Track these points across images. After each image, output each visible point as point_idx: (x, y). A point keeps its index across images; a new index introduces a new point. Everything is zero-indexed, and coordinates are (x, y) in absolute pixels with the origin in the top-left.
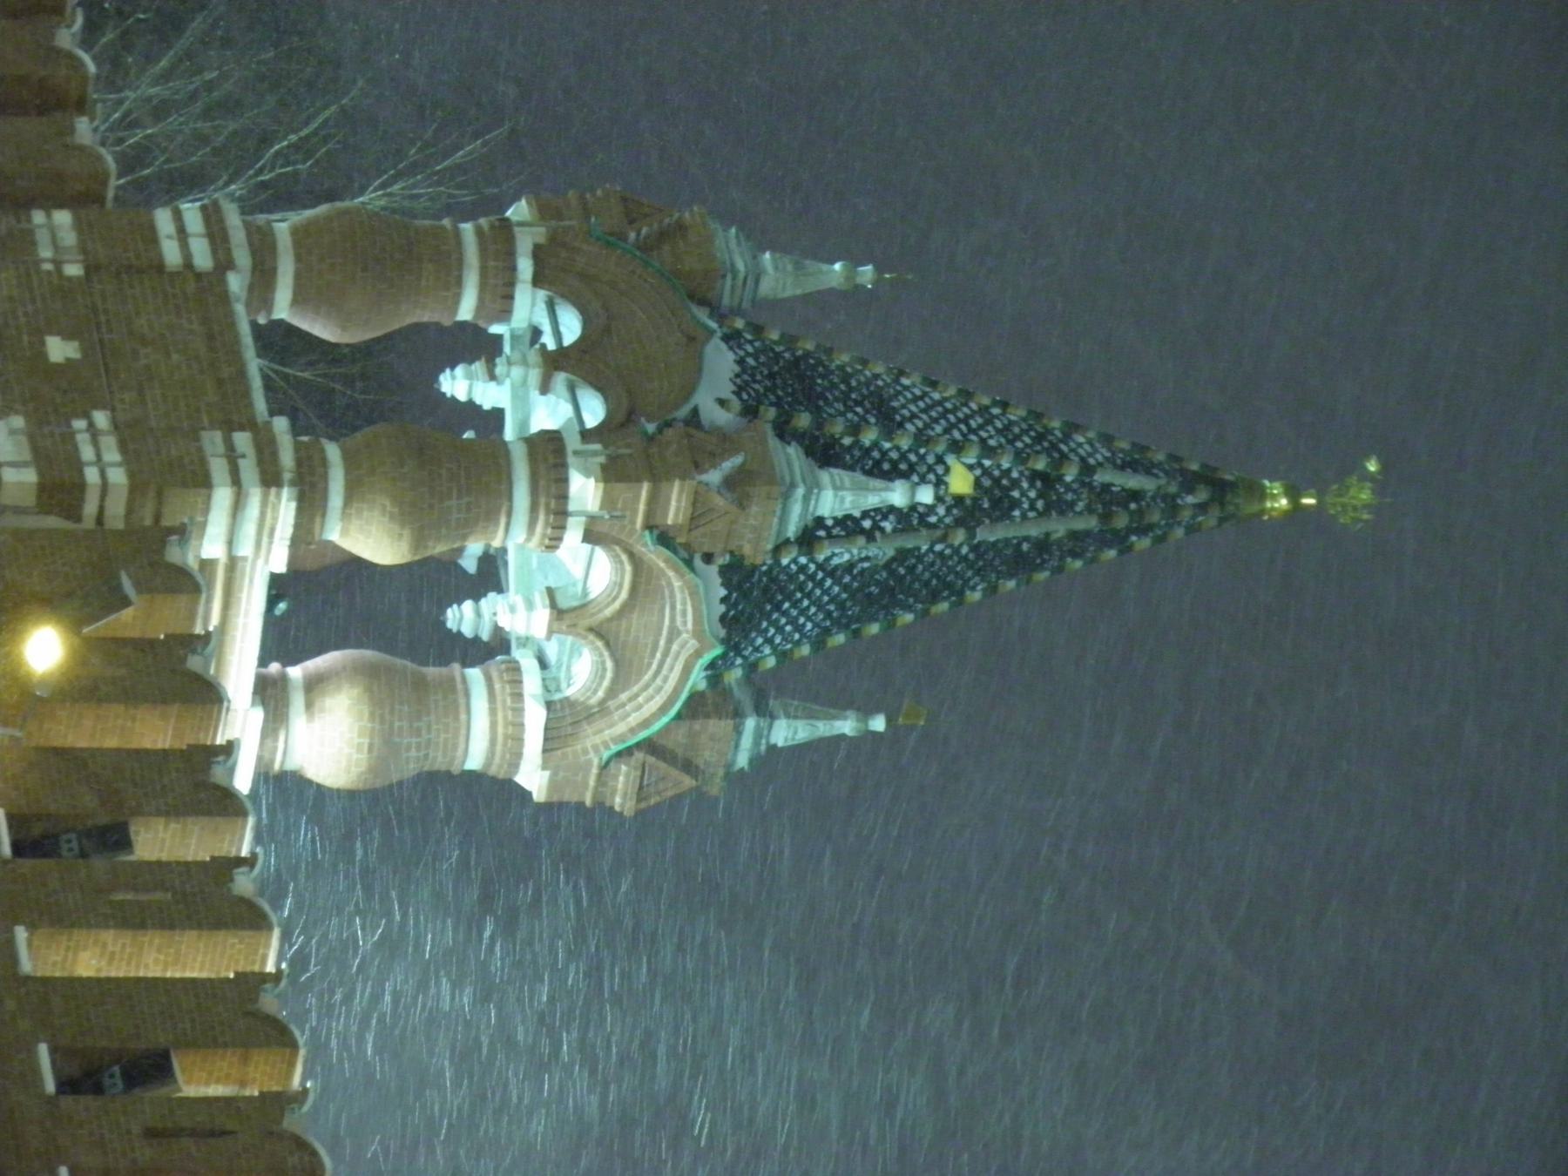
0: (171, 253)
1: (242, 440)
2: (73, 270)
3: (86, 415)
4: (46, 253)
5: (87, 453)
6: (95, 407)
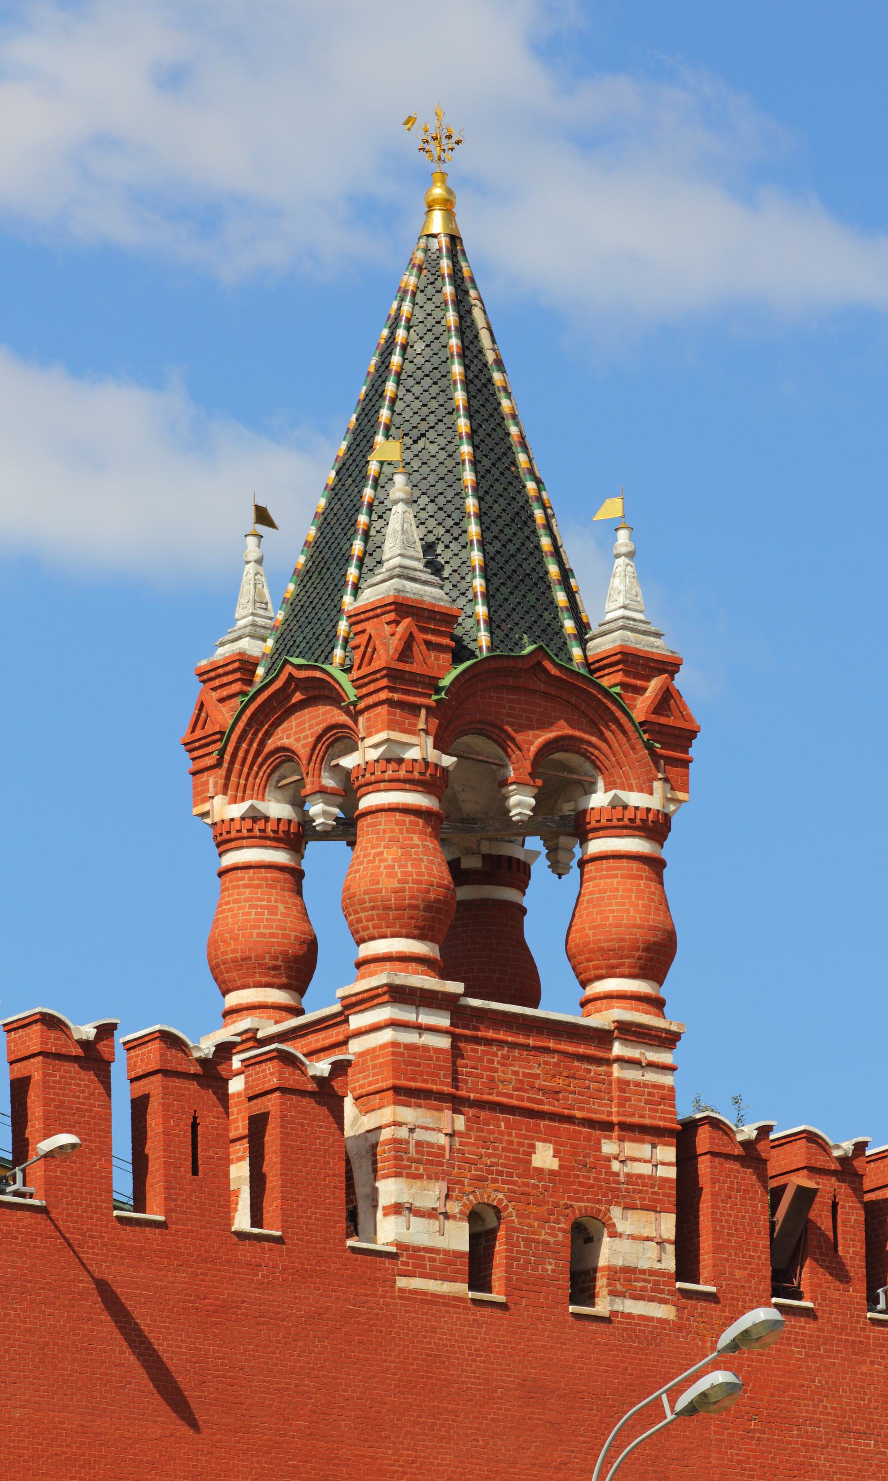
2: (460, 1123)
3: (608, 1159)
5: (645, 1169)
6: (599, 1149)
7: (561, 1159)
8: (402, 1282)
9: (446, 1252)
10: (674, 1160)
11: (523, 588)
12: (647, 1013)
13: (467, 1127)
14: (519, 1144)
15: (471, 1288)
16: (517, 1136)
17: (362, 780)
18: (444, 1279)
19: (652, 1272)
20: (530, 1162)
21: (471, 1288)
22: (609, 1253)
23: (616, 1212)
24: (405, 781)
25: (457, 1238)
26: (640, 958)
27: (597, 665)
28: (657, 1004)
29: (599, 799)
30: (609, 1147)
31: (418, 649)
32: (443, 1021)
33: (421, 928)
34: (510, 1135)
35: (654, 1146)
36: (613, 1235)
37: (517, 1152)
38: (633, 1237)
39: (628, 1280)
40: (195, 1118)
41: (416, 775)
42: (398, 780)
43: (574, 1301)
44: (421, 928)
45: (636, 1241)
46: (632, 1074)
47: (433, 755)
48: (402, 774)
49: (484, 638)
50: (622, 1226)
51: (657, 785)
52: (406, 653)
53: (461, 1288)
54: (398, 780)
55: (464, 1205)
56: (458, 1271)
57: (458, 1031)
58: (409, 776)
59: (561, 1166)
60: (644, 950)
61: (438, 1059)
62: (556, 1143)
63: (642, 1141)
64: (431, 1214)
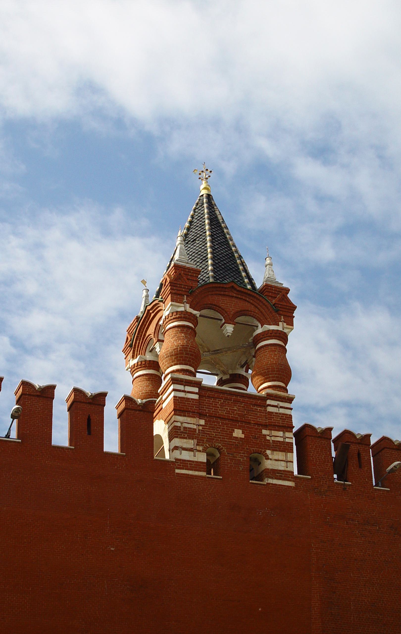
0: (196, 397)
1: (269, 402)
2: (202, 422)
4: (195, 427)
5: (281, 439)
8: (177, 471)
18: (195, 470)
19: (284, 471)
38: (276, 460)
56: (202, 468)
64: (191, 450)
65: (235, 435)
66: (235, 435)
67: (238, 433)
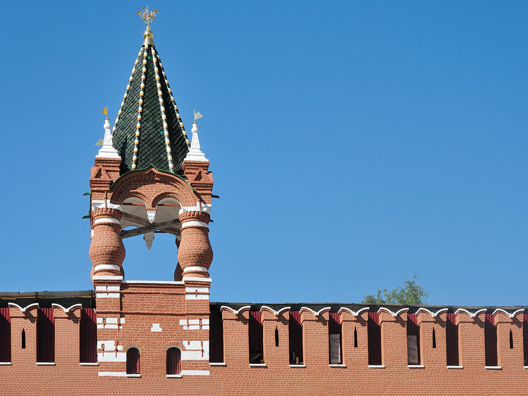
1: (188, 290)
3: (182, 326)
7: (163, 328)
9: (118, 363)
10: (208, 323)
11: (154, 148)
12: (202, 277)
13: (126, 322)
14: (146, 325)
15: (127, 373)
16: (145, 322)
17: (181, 219)
20: (150, 330)
21: (127, 373)
22: (185, 356)
23: (185, 343)
24: (105, 215)
25: (122, 357)
26: (192, 259)
27: (116, 165)
28: (206, 275)
29: (181, 212)
30: (183, 322)
31: (103, 172)
32: (117, 288)
33: (109, 260)
34: (143, 322)
35: (188, 319)
36: (184, 350)
37: (145, 327)
39: (194, 365)
40: (434, 330)
41: (104, 212)
42: (103, 215)
43: (168, 373)
44: (109, 260)
45: (196, 351)
46: (105, 296)
47: (110, 206)
48: (100, 213)
49: (134, 166)
50: (187, 347)
51: (198, 203)
52: (99, 175)
53: (124, 374)
54: (103, 215)
55: (125, 347)
56: (122, 368)
57: (123, 291)
58: (102, 213)
59: (163, 330)
60: (193, 257)
61: (114, 301)
62: (160, 323)
63: (196, 319)
65: (153, 330)
66: (153, 330)
67: (156, 328)
